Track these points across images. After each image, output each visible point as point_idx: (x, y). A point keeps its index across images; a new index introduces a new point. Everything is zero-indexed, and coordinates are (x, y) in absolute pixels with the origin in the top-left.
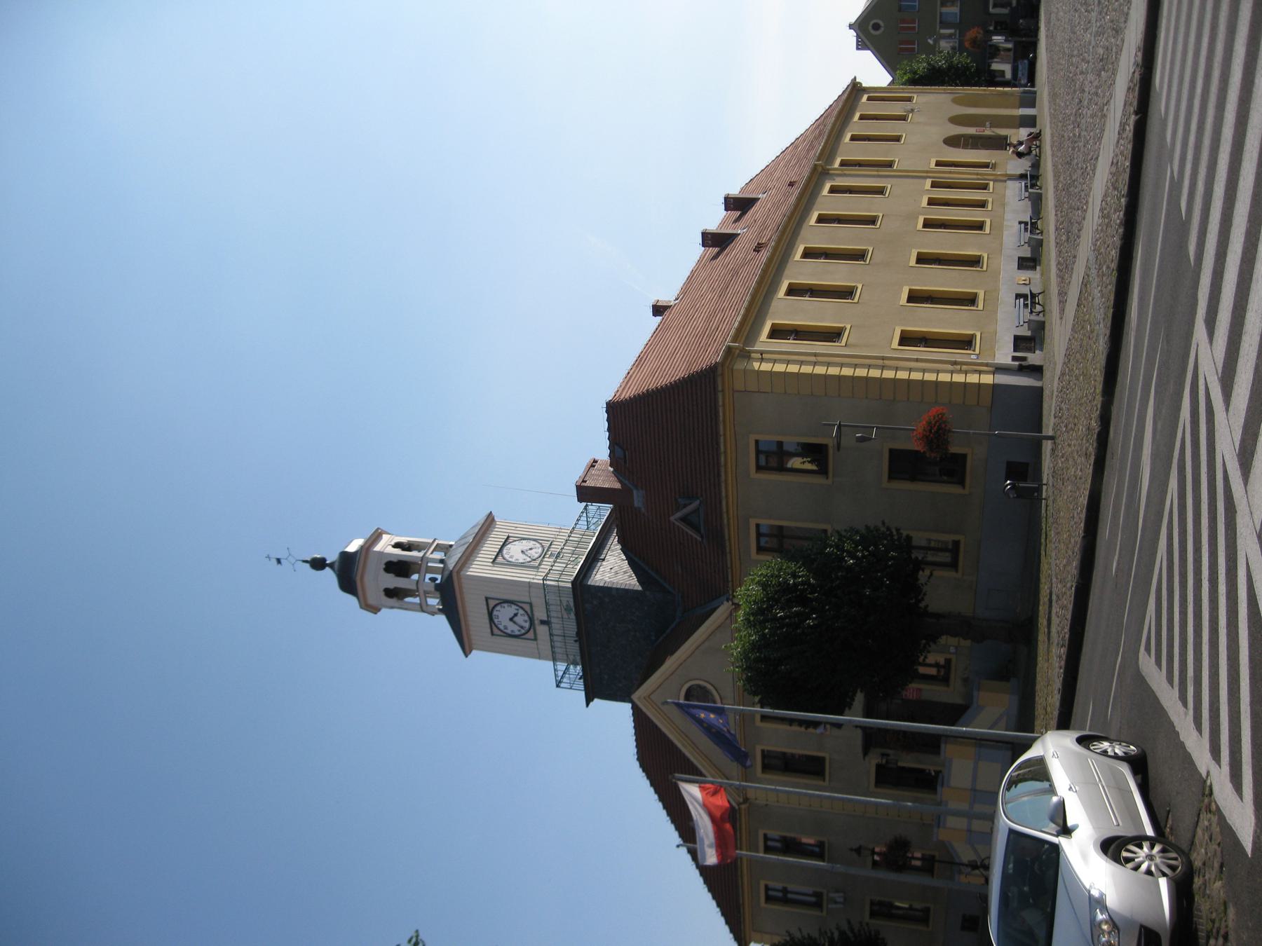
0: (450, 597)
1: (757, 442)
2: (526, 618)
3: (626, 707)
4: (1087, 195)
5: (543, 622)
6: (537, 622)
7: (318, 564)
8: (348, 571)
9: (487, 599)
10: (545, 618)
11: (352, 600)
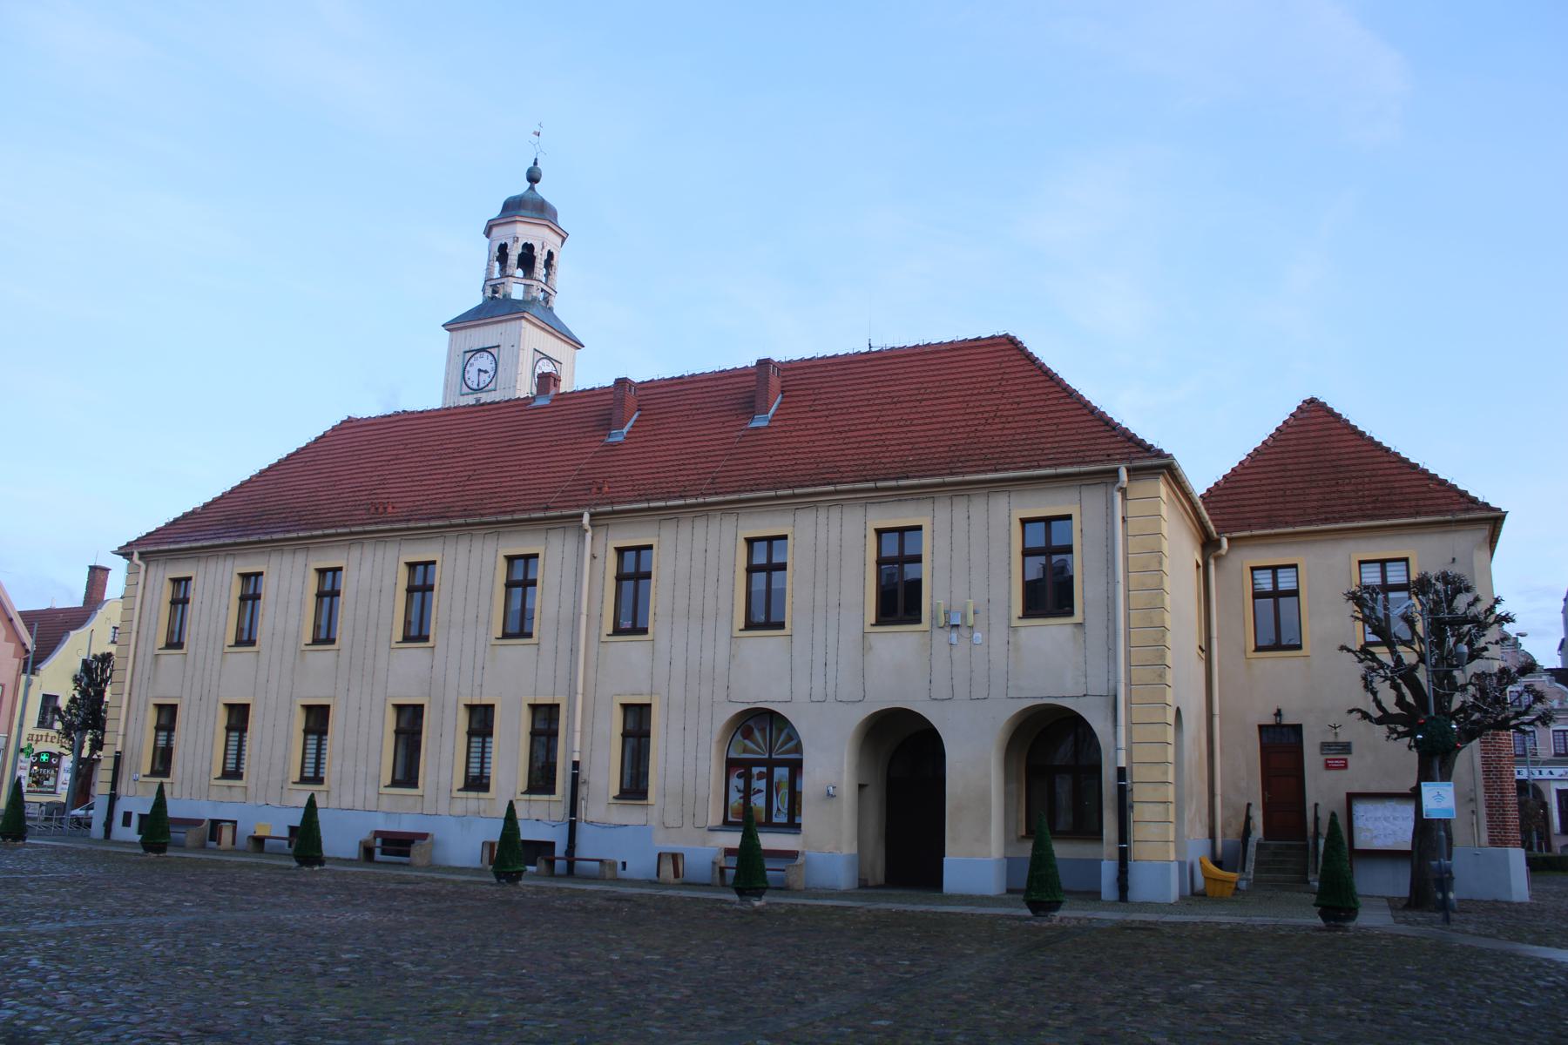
7: (533, 177)
11: (495, 212)
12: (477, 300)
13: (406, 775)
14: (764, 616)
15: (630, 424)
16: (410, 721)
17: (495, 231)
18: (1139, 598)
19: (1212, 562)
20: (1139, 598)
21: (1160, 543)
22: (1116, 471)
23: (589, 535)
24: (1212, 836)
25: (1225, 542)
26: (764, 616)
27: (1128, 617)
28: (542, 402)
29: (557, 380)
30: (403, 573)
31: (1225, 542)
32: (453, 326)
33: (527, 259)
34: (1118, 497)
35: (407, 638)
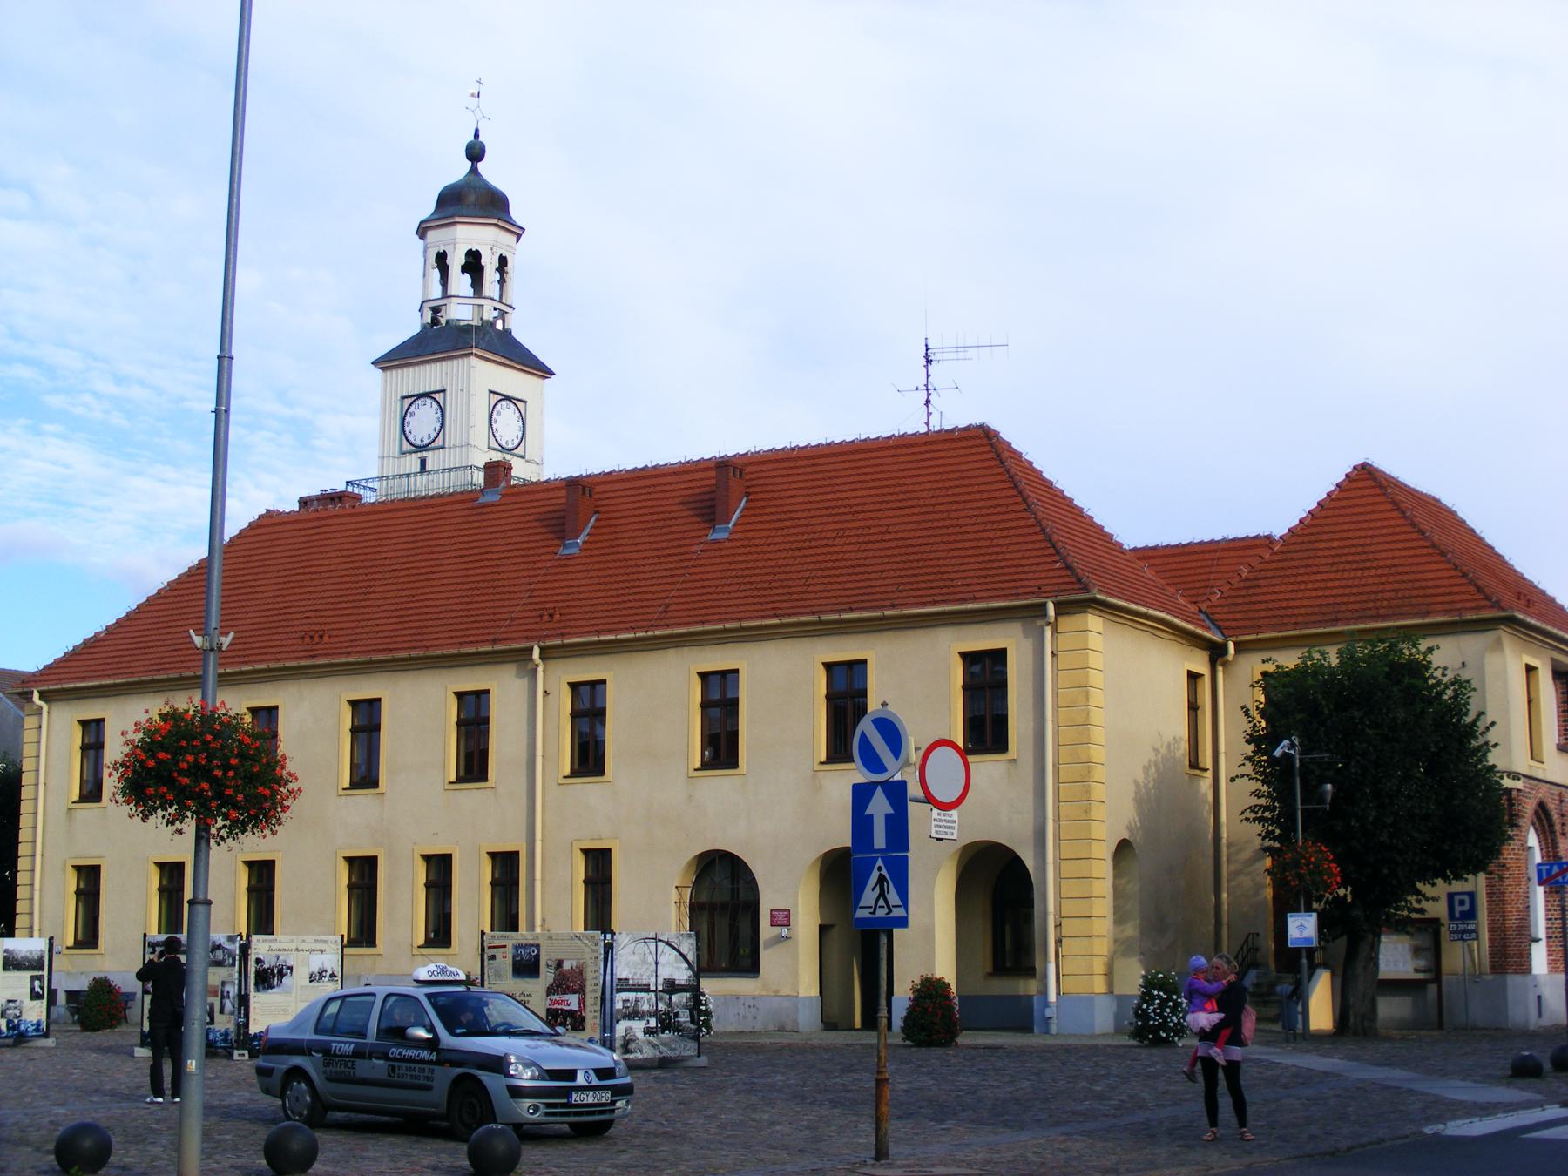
0: (438, 340)
1: (604, 682)
2: (426, 441)
3: (849, 843)
4: (1006, 1124)
5: (423, 462)
6: (425, 454)
7: (475, 153)
8: (469, 199)
9: (444, 391)
10: (429, 468)
11: (428, 208)
12: (411, 326)
13: (363, 932)
14: (721, 749)
15: (587, 531)
16: (364, 872)
17: (430, 234)
18: (1067, 734)
19: (1220, 669)
20: (1067, 734)
21: (1087, 677)
22: (1044, 605)
23: (540, 669)
24: (687, 961)
25: (1231, 646)
26: (721, 749)
27: (1057, 753)
28: (492, 497)
29: (507, 468)
30: (347, 713)
31: (1231, 646)
32: (388, 362)
33: (473, 264)
34: (1048, 631)
35: (354, 785)
